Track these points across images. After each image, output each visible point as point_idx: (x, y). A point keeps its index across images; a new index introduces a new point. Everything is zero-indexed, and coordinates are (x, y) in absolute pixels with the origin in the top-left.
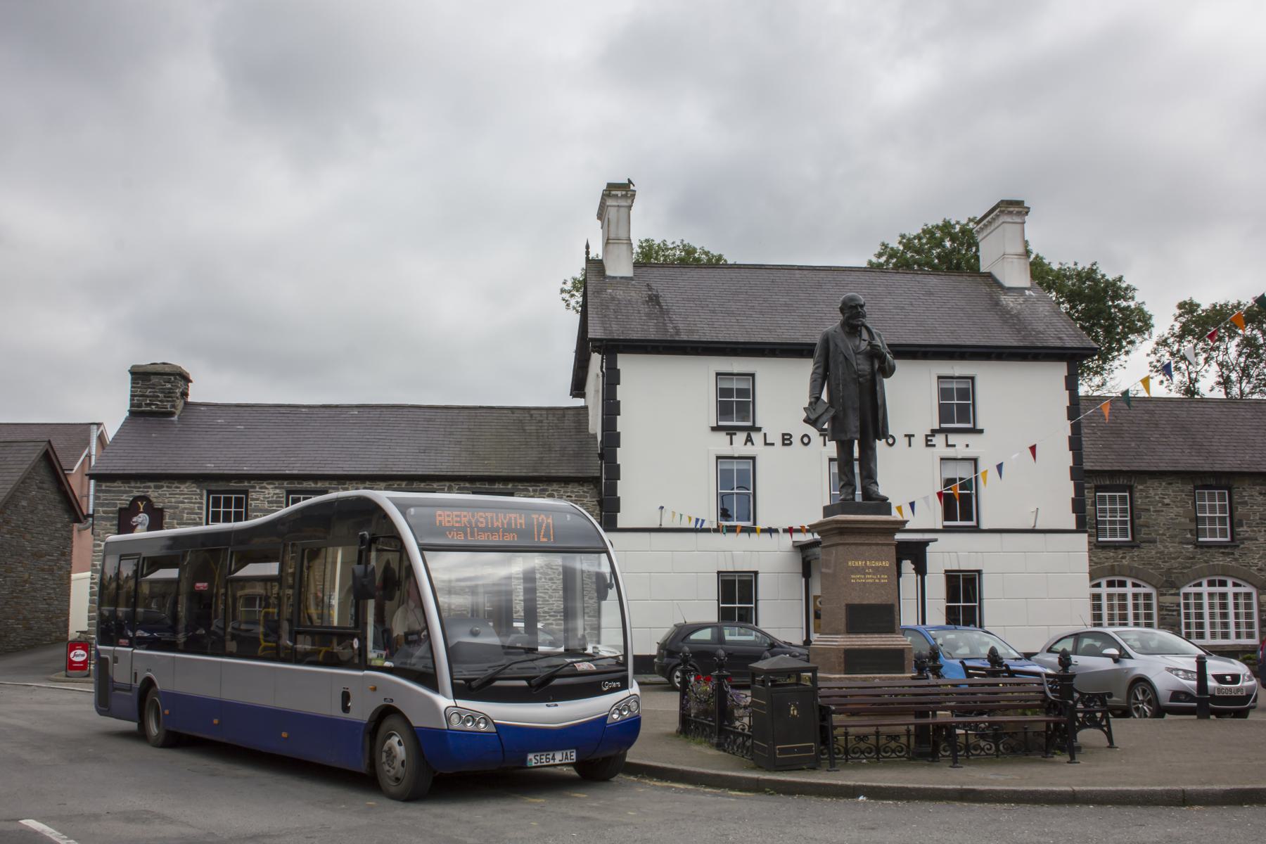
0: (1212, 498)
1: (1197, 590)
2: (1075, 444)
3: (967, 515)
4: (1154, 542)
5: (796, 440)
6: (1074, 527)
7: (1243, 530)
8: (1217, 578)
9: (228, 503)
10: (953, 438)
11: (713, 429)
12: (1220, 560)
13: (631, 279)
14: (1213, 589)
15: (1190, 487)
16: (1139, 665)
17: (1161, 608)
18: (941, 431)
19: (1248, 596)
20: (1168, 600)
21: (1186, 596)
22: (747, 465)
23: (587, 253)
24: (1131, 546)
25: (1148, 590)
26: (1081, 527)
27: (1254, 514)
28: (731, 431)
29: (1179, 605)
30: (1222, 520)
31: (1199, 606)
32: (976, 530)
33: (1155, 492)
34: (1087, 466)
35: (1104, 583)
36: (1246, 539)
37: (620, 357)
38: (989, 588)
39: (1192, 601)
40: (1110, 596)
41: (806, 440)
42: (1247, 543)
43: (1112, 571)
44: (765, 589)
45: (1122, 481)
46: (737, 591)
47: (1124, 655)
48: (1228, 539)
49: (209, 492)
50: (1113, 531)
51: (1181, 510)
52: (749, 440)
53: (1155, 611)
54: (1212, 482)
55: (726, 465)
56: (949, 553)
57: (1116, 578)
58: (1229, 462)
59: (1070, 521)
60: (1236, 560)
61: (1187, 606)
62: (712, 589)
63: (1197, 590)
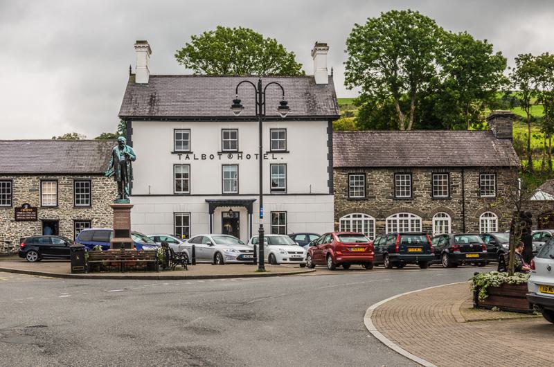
0: (403, 178)
1: (395, 218)
2: (330, 157)
3: (186, 189)
4: (375, 197)
5: (208, 157)
6: (328, 193)
7: (417, 192)
8: (357, 214)
9: (82, 185)
10: (276, 155)
11: (172, 153)
12: (405, 205)
13: (147, 84)
14: (355, 219)
15: (392, 173)
16: (217, 247)
17: (377, 227)
18: (271, 152)
19: (372, 221)
20: (426, 222)
21: (389, 221)
22: (234, 169)
23: (130, 71)
24: (363, 200)
25: (418, 218)
26: (332, 192)
27: (422, 185)
28: (180, 153)
29: (385, 225)
30: (408, 188)
31: (395, 226)
32: (189, 195)
33: (376, 175)
34: (335, 165)
35: (398, 215)
36: (417, 196)
37: (132, 122)
38: (290, 218)
39: (392, 223)
40: (354, 222)
41: (212, 157)
42: (418, 198)
43: (355, 211)
44: (194, 220)
45: (408, 171)
46: (182, 224)
47: (212, 244)
48: (410, 196)
49: (75, 181)
50: (403, 194)
51: (388, 184)
52: (187, 157)
53: (374, 228)
54: (403, 171)
55: (226, 169)
56: (273, 204)
57: (357, 214)
58: (413, 161)
59: (327, 190)
60: (412, 205)
61: (390, 226)
62: (171, 219)
63: (395, 218)
